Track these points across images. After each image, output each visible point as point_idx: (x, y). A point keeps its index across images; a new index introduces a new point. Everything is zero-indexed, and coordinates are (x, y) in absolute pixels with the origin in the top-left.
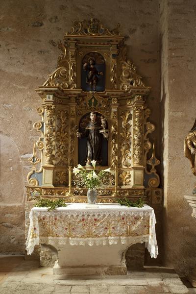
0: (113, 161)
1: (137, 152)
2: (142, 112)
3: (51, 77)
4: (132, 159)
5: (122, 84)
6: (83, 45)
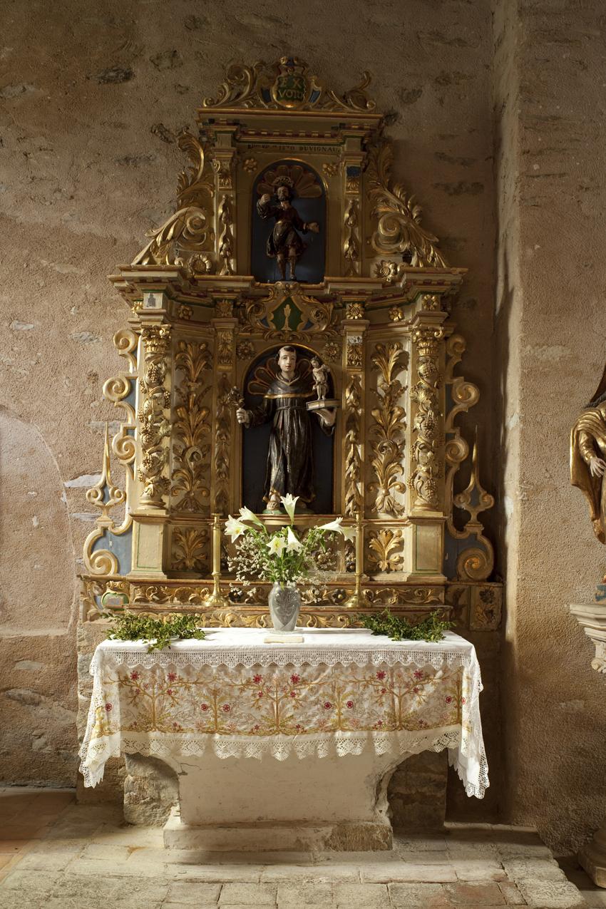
0: (348, 496)
1: (424, 469)
2: (438, 347)
3: (159, 239)
4: (408, 490)
5: (379, 259)
6: (257, 139)
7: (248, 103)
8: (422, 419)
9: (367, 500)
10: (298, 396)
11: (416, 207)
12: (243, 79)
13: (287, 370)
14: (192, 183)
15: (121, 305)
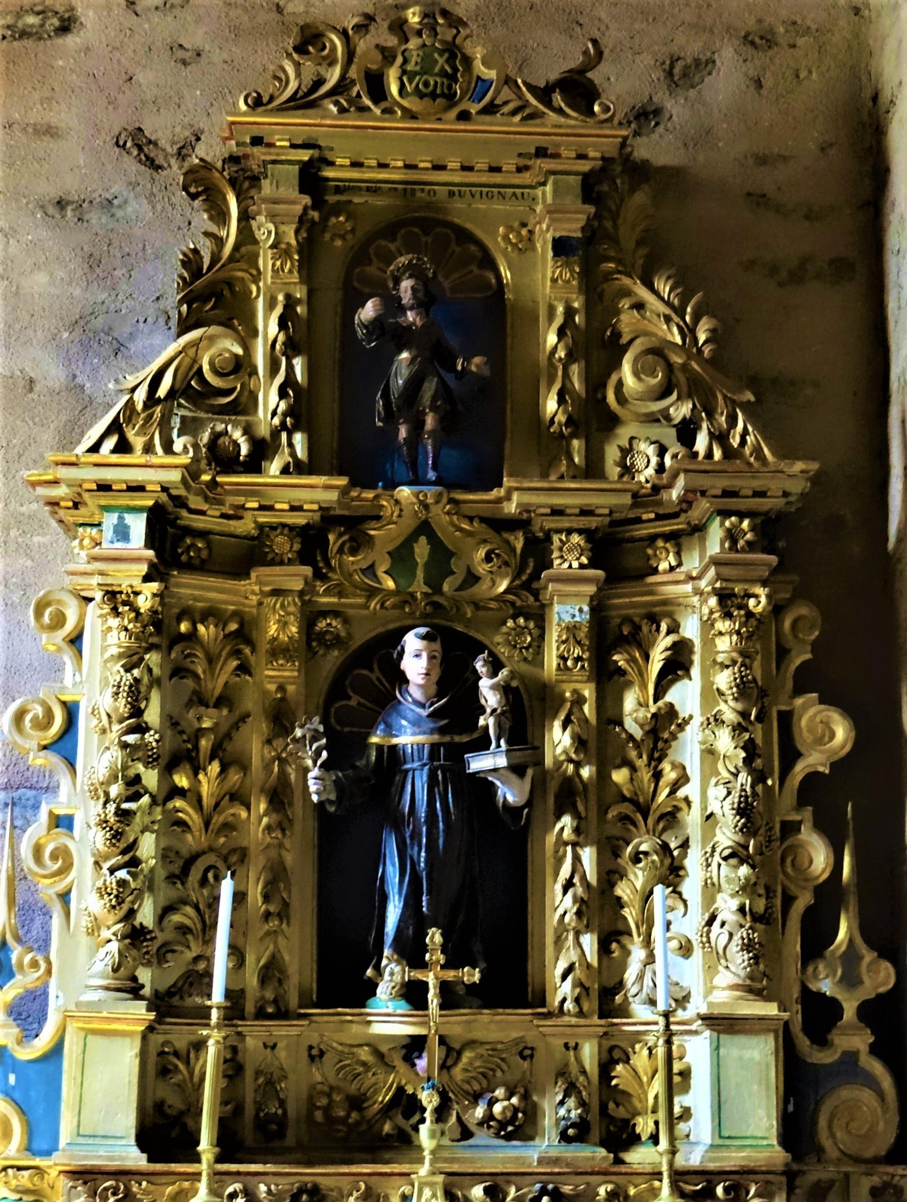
0: (562, 965)
1: (734, 904)
2: (758, 635)
3: (140, 396)
4: (698, 953)
5: (623, 434)
6: (355, 174)
7: (336, 103)
8: (725, 792)
9: (605, 974)
10: (447, 739)
11: (704, 320)
12: (326, 52)
13: (422, 682)
14: (210, 268)
15: (42, 527)
